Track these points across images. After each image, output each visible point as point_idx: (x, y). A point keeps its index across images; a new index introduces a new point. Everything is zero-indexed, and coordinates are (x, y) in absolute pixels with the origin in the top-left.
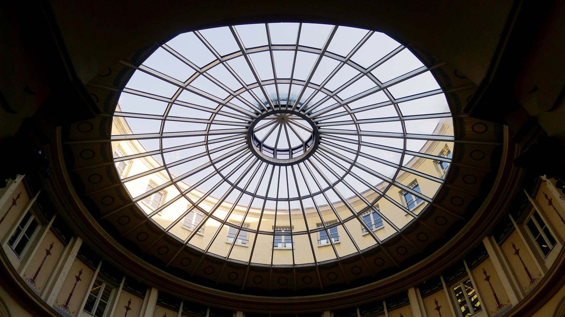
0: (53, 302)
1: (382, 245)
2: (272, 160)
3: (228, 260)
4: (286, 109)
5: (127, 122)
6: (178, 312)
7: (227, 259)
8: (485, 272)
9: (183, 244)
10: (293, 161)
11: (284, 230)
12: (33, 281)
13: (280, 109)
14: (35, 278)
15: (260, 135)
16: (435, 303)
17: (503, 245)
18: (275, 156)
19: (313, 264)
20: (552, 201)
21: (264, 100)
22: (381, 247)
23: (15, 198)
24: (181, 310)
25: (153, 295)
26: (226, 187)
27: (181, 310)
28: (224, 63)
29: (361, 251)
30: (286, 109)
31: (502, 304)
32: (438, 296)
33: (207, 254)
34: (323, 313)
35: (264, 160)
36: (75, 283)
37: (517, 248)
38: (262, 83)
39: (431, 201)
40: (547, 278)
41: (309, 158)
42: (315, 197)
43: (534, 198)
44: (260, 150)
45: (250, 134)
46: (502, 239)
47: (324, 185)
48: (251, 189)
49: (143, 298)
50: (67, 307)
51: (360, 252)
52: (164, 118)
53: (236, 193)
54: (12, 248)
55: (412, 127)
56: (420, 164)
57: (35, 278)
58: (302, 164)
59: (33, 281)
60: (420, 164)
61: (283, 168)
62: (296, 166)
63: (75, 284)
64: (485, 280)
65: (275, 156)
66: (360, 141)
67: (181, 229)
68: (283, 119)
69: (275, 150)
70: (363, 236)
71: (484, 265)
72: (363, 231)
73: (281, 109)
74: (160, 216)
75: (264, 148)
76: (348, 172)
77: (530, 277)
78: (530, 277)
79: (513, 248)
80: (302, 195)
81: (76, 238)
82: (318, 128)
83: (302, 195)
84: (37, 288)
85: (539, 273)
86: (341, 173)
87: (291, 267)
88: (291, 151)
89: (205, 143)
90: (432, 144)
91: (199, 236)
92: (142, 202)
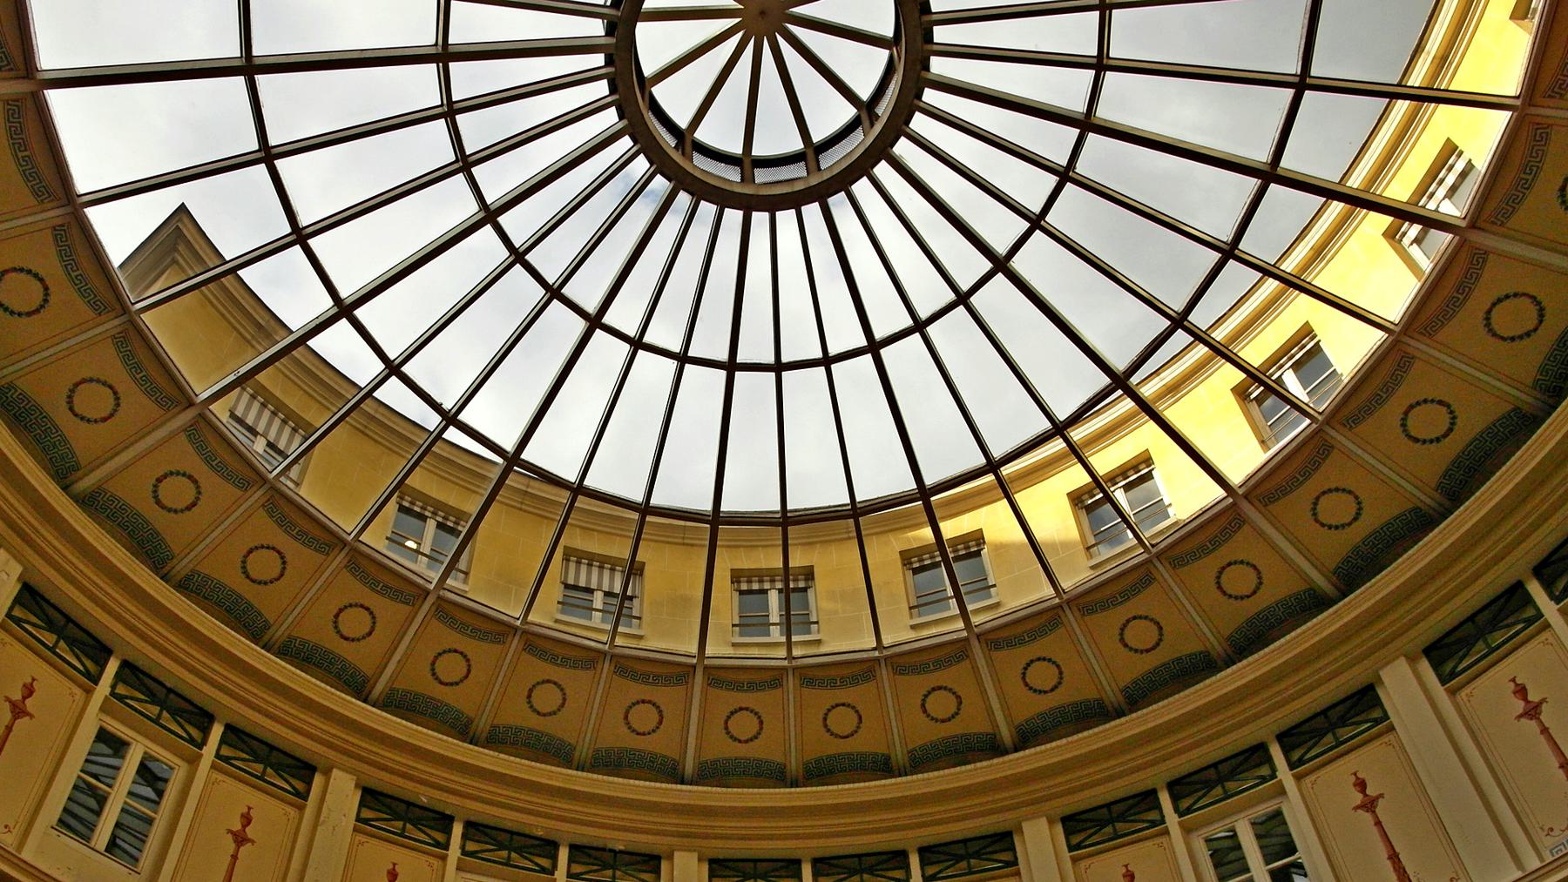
18: (747, 178)
34: (1380, 680)
44: (683, 154)
69: (746, 162)
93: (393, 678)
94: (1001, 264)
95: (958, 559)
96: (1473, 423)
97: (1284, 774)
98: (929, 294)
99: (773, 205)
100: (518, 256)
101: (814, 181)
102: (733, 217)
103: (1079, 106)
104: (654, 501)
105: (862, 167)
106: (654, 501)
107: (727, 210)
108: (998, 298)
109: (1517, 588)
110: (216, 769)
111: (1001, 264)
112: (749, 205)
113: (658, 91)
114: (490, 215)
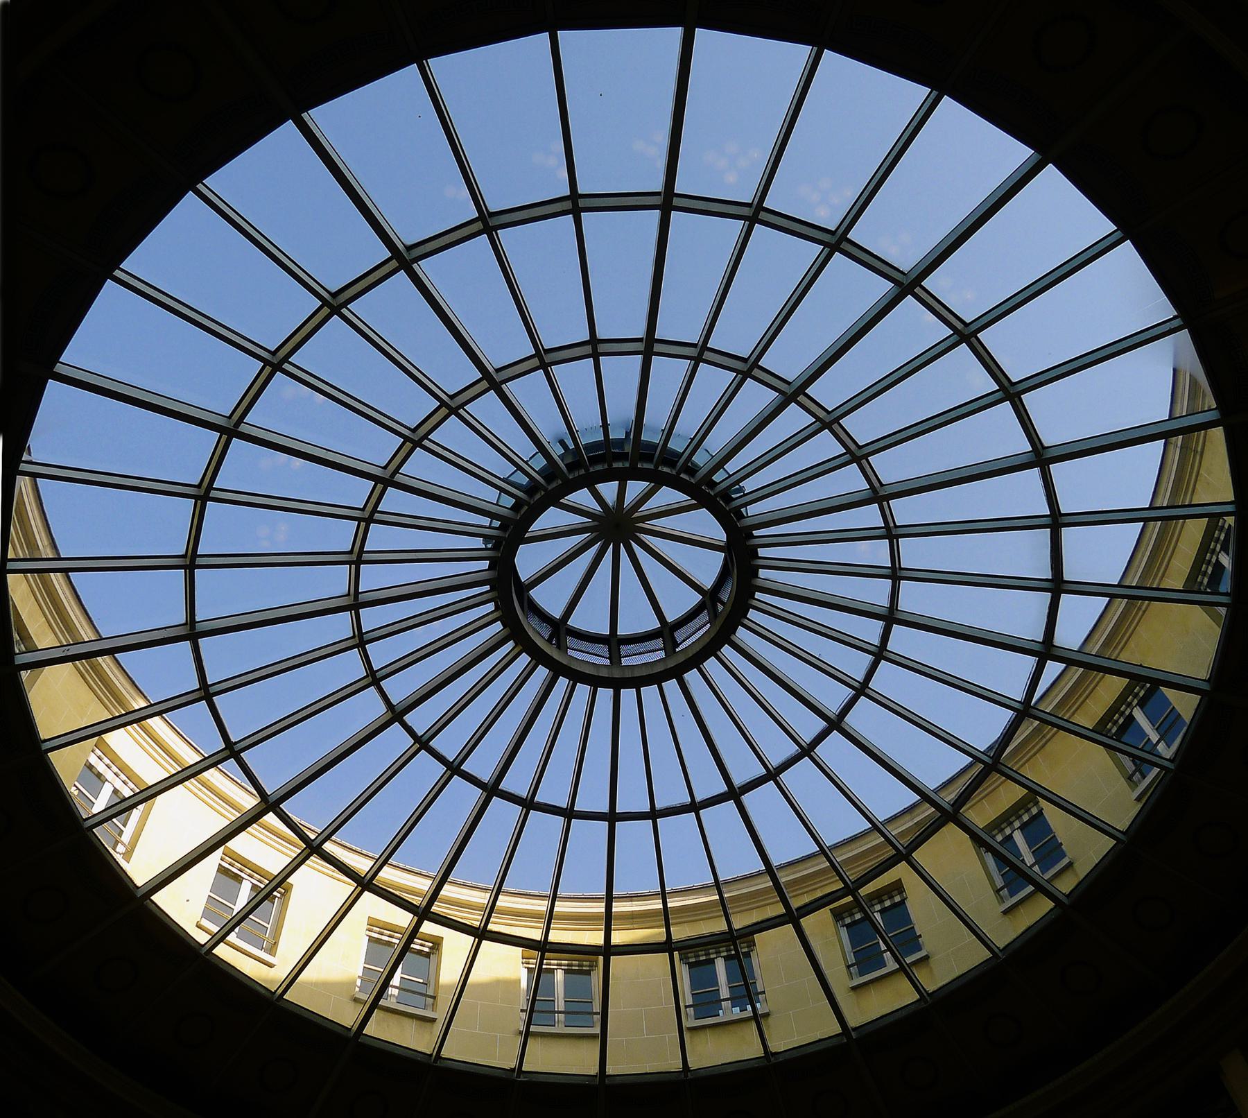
2: (604, 673)
3: (522, 1079)
4: (606, 467)
5: (133, 683)
7: (518, 1076)
11: (723, 954)
13: (587, 470)
18: (615, 657)
19: (840, 1038)
28: (426, 442)
29: (1001, 951)
30: (606, 467)
35: (577, 677)
38: (498, 377)
39: (1206, 687)
41: (733, 637)
42: (784, 777)
44: (559, 647)
47: (809, 726)
48: (554, 792)
51: (1000, 955)
53: (502, 814)
56: (1141, 613)
60: (1141, 613)
62: (692, 677)
65: (615, 657)
66: (892, 525)
67: (352, 1004)
69: (613, 642)
70: (1005, 912)
72: (1002, 898)
73: (591, 470)
74: (271, 966)
75: (570, 641)
76: (880, 654)
80: (738, 781)
82: (722, 498)
83: (738, 781)
86: (855, 664)
88: (666, 632)
89: (357, 641)
91: (418, 1022)
92: (197, 926)
98: (855, 664)
99: (638, 682)
101: (671, 663)
102: (605, 694)
104: (621, 631)
105: (710, 649)
106: (621, 631)
107: (699, 33)
112: (617, 685)
114: (396, 714)
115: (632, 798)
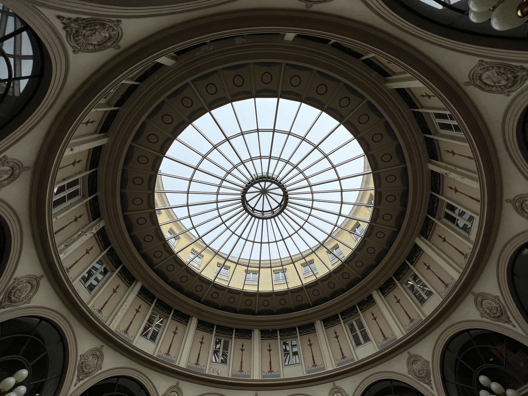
0: (115, 326)
1: (344, 262)
6: (212, 334)
8: (425, 264)
9: (212, 282)
10: (274, 214)
12: (100, 311)
14: (102, 309)
15: (252, 203)
16: (451, 189)
17: (431, 240)
18: (263, 214)
20: (457, 189)
21: (251, 179)
22: (344, 264)
23: (78, 217)
24: (214, 332)
25: (194, 323)
26: (235, 238)
27: (214, 332)
31: (466, 254)
32: (395, 292)
33: (228, 287)
34: (316, 323)
35: (256, 217)
36: (135, 314)
37: (443, 237)
40: (476, 248)
43: (442, 195)
45: (244, 202)
46: (414, 261)
49: (187, 325)
50: (127, 332)
52: (190, 180)
54: (53, 210)
55: (343, 171)
57: (102, 309)
58: (280, 216)
59: (100, 311)
61: (269, 220)
62: (276, 218)
63: (135, 315)
64: (427, 269)
68: (264, 191)
69: (263, 212)
71: (423, 259)
75: (255, 211)
77: (445, 284)
78: (445, 284)
79: (440, 238)
81: (137, 281)
84: (103, 316)
85: (467, 246)
87: (287, 290)
90: (349, 221)
93: (205, 298)
94: (312, 208)
95: (310, 264)
96: (336, 288)
97: (298, 334)
99: (267, 219)
100: (228, 228)
103: (301, 225)
105: (280, 213)
108: (314, 212)
109: (337, 315)
110: (282, 340)
111: (312, 208)
112: (263, 219)
113: (249, 203)
114: (224, 223)
115: (265, 240)
